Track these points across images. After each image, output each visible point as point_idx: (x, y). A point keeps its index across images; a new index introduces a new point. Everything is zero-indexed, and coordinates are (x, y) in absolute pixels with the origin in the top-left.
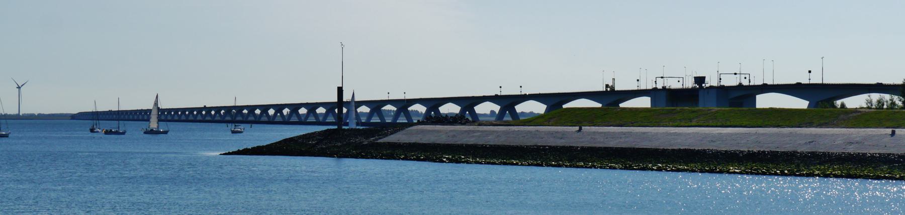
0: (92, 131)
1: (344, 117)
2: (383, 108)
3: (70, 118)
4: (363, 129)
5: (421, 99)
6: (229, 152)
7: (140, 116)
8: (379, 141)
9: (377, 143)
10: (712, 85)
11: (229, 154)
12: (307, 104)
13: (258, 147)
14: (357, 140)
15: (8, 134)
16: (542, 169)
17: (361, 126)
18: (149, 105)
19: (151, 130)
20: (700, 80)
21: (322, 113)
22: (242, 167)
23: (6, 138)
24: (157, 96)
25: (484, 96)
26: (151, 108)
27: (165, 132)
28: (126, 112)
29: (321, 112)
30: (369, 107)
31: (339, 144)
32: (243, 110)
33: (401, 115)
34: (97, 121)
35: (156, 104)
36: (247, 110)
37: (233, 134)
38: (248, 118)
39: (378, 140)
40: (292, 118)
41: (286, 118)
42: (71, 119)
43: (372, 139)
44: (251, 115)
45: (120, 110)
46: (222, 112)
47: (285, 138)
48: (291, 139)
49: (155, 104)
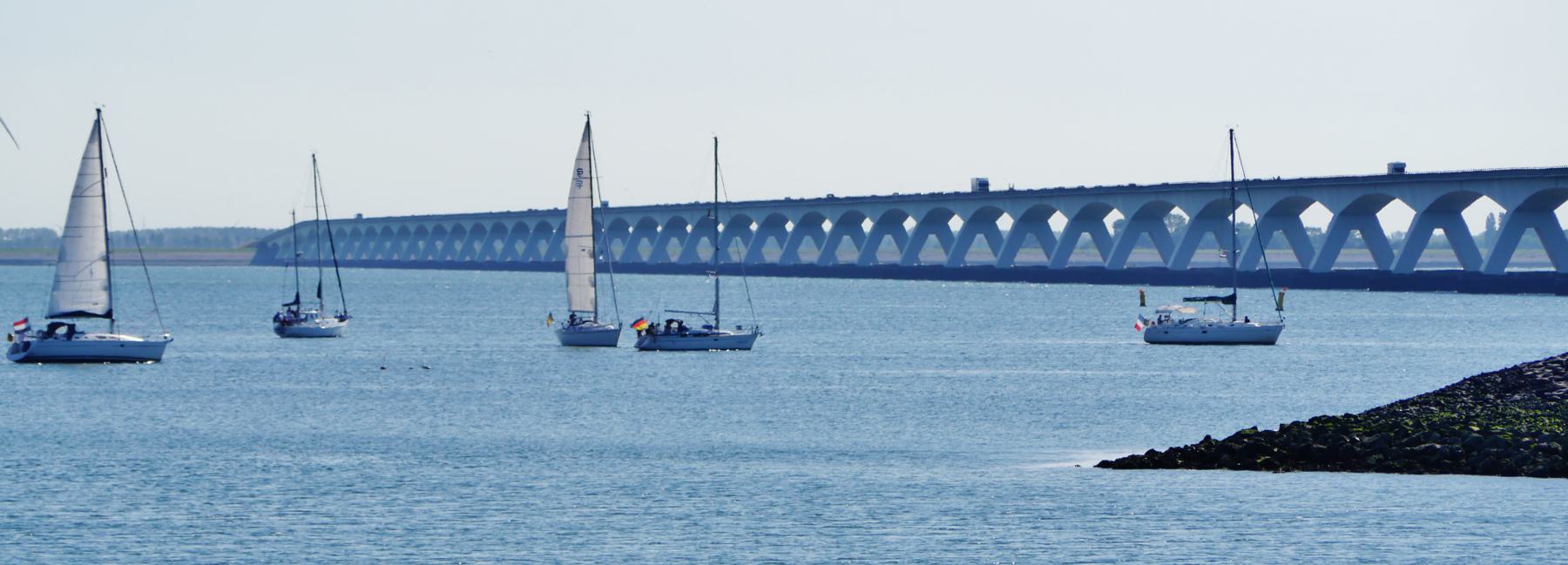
0: (288, 325)
3: (251, 254)
6: (1151, 453)
7: (645, 241)
10: (729, 200)
11: (1153, 461)
13: (1320, 423)
15: (161, 346)
16: (1513, 482)
18: (551, 194)
19: (1181, 322)
20: (360, 215)
22: (1272, 521)
24: (98, 123)
28: (157, 237)
30: (1331, 210)
34: (329, 272)
35: (583, 174)
37: (573, 351)
41: (1485, 253)
42: (256, 262)
45: (721, 199)
46: (1113, 218)
47: (1476, 372)
48: (1514, 380)
49: (579, 171)
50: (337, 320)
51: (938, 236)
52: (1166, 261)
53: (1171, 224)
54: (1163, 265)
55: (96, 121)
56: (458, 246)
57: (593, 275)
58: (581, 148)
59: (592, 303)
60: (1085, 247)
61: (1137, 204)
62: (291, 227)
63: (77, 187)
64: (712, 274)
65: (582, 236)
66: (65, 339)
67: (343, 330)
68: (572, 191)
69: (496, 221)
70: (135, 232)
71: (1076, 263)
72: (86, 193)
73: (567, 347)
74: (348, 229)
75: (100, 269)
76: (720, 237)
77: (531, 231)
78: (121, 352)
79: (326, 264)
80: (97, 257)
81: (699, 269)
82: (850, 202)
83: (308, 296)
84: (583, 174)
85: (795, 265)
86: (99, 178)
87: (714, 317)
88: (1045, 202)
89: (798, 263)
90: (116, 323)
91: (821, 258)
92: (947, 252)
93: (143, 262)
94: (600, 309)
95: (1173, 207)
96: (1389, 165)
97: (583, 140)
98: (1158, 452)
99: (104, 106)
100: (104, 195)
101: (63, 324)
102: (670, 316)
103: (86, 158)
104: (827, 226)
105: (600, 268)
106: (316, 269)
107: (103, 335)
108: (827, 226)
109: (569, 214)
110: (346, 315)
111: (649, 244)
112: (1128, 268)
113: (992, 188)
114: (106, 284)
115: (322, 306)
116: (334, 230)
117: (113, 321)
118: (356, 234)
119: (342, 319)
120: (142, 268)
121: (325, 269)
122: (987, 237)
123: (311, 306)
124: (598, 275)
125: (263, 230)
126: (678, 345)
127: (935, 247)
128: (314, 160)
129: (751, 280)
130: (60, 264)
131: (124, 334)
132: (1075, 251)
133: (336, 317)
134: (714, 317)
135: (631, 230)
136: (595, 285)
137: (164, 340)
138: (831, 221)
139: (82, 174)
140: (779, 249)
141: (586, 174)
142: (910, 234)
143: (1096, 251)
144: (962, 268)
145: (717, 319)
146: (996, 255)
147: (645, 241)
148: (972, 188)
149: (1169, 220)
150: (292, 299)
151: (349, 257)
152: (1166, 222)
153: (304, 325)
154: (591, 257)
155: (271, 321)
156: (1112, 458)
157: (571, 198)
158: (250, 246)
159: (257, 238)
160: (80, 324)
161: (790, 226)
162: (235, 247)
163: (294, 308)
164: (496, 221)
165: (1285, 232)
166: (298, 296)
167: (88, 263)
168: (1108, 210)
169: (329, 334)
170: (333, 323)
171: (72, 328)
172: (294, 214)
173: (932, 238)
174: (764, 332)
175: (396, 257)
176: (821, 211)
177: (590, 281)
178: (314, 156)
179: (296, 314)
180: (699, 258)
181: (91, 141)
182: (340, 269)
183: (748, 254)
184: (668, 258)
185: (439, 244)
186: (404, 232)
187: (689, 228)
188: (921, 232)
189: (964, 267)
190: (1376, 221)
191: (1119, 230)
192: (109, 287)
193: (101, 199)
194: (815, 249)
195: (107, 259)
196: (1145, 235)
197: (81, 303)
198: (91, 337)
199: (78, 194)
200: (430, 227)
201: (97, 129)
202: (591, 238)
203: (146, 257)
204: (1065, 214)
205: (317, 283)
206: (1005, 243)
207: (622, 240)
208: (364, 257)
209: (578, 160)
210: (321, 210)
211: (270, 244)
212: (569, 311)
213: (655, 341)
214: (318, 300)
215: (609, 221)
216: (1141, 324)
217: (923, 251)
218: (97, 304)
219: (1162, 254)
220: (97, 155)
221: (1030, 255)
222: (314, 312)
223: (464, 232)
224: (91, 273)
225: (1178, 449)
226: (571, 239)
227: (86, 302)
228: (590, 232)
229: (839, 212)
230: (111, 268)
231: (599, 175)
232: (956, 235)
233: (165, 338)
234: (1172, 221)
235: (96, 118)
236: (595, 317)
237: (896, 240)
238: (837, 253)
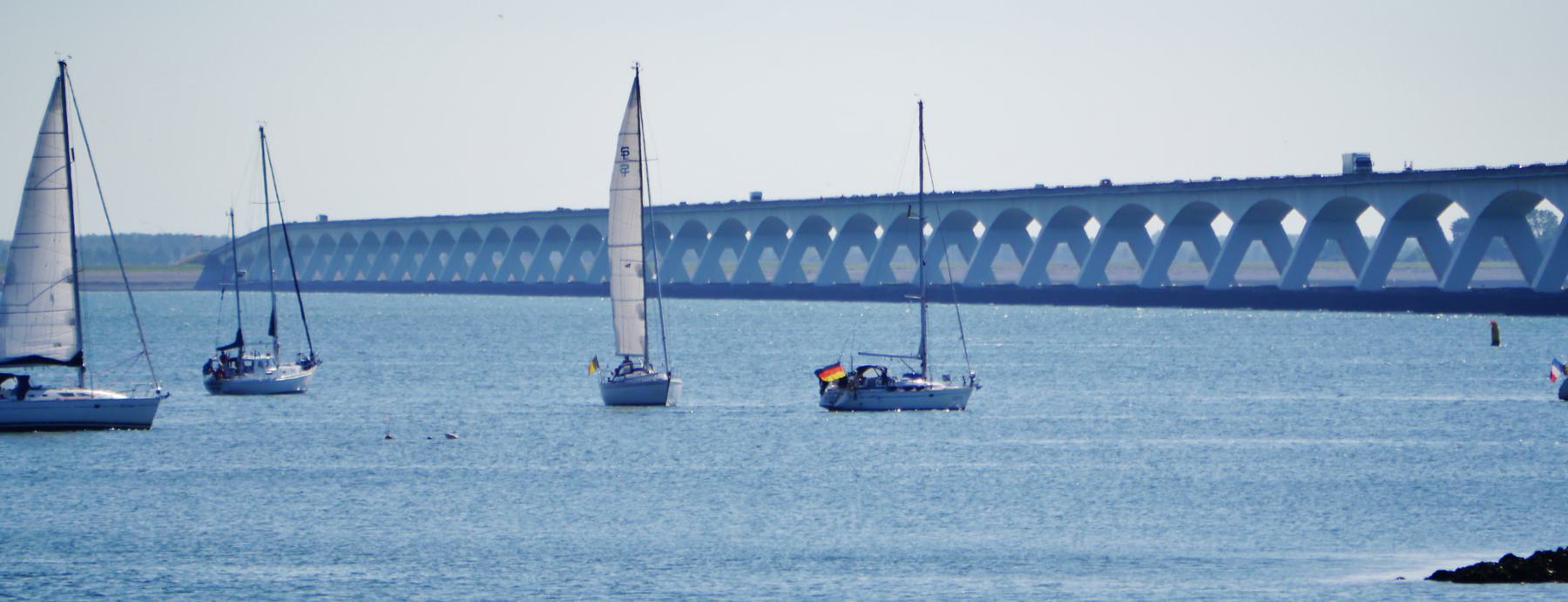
3: (197, 273)
5: (589, 210)
6: (1509, 559)
12: (1480, 175)
15: (151, 405)
23: (139, 434)
24: (61, 82)
25: (1272, 178)
26: (599, 199)
34: (287, 299)
35: (629, 157)
45: (927, 190)
46: (1451, 217)
49: (624, 151)
50: (299, 367)
51: (1196, 244)
52: (1529, 278)
53: (1537, 225)
54: (1526, 285)
55: (58, 78)
56: (498, 260)
57: (643, 302)
58: (626, 122)
59: (641, 342)
60: (1412, 258)
61: (1487, 196)
62: (262, 230)
63: (32, 175)
64: (915, 301)
65: (628, 246)
66: (15, 397)
67: (307, 382)
68: (615, 180)
69: (687, 218)
70: (113, 237)
71: (1396, 282)
72: (40, 186)
73: (612, 407)
74: (315, 237)
75: (65, 293)
76: (926, 249)
77: (572, 240)
78: (96, 415)
79: (282, 286)
80: (60, 277)
81: (896, 293)
82: (1011, 196)
83: (256, 332)
84: (629, 157)
85: (988, 287)
86: (63, 162)
87: (921, 361)
88: (1435, 190)
89: (993, 283)
90: (87, 374)
91: (1084, 276)
92: (1208, 266)
93: (128, 286)
94: (931, 352)
95: (1538, 199)
96: (1344, 157)
97: (630, 105)
98: (1518, 558)
99: (70, 57)
100: (70, 187)
101: (11, 376)
102: (862, 362)
103: (44, 133)
104: (1034, 229)
105: (650, 291)
106: (268, 294)
107: (69, 391)
108: (1034, 229)
109: (610, 213)
110: (313, 359)
111: (775, 256)
112: (1473, 289)
113: (1376, 168)
114: (73, 315)
115: (276, 347)
116: (294, 238)
117: (83, 369)
118: (326, 243)
119: (306, 365)
120: (294, 295)
121: (280, 295)
122: (1265, 243)
123: (258, 348)
124: (649, 301)
125: (213, 238)
126: (874, 403)
127: (1192, 260)
128: (263, 137)
129: (966, 309)
130: (7, 288)
131: (99, 388)
132: (1396, 265)
133: (297, 364)
134: (921, 361)
135: (790, 234)
136: (645, 316)
137: (156, 395)
138: (1040, 221)
139: (39, 157)
140: (964, 262)
141: (633, 155)
142: (1155, 241)
143: (1427, 265)
144: (1163, 289)
145: (923, 365)
146: (1280, 270)
147: (811, 252)
148: (1344, 169)
149: (1534, 219)
150: (232, 339)
151: (318, 276)
152: (1530, 221)
153: (249, 377)
154: (639, 275)
155: (199, 372)
156: (1452, 566)
157: (614, 190)
158: (195, 261)
159: (207, 251)
160: (38, 375)
161: (979, 230)
162: (172, 263)
163: (234, 353)
164: (687, 218)
165: (1507, 239)
166: (239, 334)
167: (47, 286)
168: (1443, 204)
169: (289, 389)
170: (296, 372)
171: (24, 380)
172: (232, 215)
173: (1188, 247)
174: (980, 384)
175: (407, 277)
176: (1026, 207)
177: (640, 313)
178: (261, 130)
179: (239, 360)
180: (847, 275)
181: (51, 107)
182: (133, 293)
183: (825, 269)
184: (804, 277)
185: (470, 258)
186: (418, 240)
187: (833, 233)
188: (1391, 237)
189: (1233, 287)
190: (1437, 223)
191: (1460, 234)
192: (77, 321)
193: (65, 193)
194: (1017, 262)
195: (74, 279)
196: (1499, 241)
197: (35, 344)
198: (52, 394)
199: (34, 186)
200: (483, 232)
201: (60, 93)
202: (641, 248)
203: (133, 275)
204: (1382, 211)
205: (268, 315)
206: (1293, 255)
207: (736, 251)
208: (360, 277)
209: (623, 134)
210: (274, 208)
211: (223, 259)
212: (617, 354)
213: (855, 397)
214: (271, 339)
215: (655, 222)
216: (1556, 372)
217: (1172, 266)
218: (59, 345)
219: (1523, 267)
220: (60, 128)
221: (1331, 271)
222: (263, 357)
223: (565, 237)
224: (52, 298)
225: (1549, 553)
226: (614, 249)
227: (45, 343)
228: (639, 240)
229: (1112, 207)
230: (81, 293)
231: (648, 158)
232: (1222, 242)
233: (158, 392)
234: (1539, 220)
235: (58, 73)
236: (646, 362)
237: (1135, 252)
238: (1049, 267)
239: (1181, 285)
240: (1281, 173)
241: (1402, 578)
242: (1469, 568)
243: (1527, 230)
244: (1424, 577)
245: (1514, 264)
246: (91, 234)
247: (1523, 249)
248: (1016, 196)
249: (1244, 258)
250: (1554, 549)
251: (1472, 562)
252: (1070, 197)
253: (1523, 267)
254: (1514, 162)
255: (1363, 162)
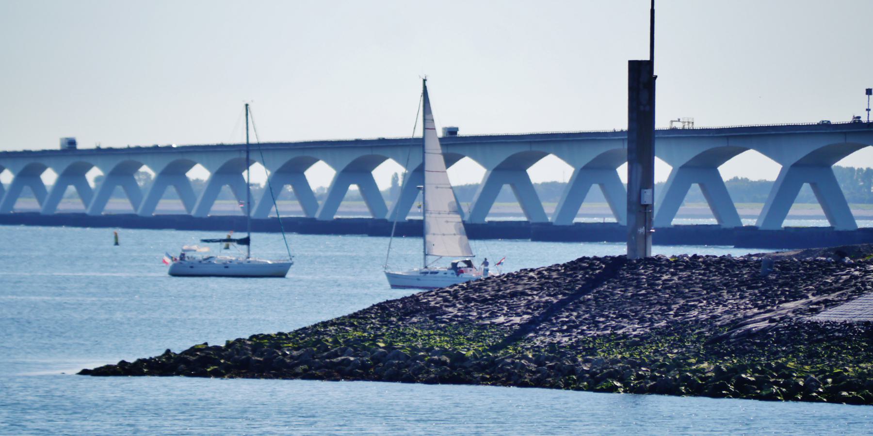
1: (657, 205)
2: (845, 163)
4: (745, 262)
6: (123, 363)
8: (821, 317)
9: (814, 325)
12: (111, 152)
13: (258, 340)
14: (720, 309)
17: (738, 245)
21: (554, 184)
27: (278, 272)
29: (549, 179)
31: (634, 329)
32: (190, 165)
33: (501, 195)
36: (207, 166)
38: (155, 203)
39: (816, 311)
40: (585, 207)
41: (390, 204)
43: (792, 305)
44: (226, 188)
45: (253, 140)
46: (93, 175)
52: (136, 208)
53: (140, 180)
54: (185, 213)
60: (71, 197)
88: (188, 157)
95: (140, 165)
152: (136, 177)
156: (91, 367)
165: (124, 187)
168: (89, 167)
216: (168, 260)
225: (144, 360)
239: (599, 243)
240: (133, 145)
241: (63, 373)
242: (101, 368)
243: (134, 182)
244: (75, 373)
245: (180, 202)
246: (660, 182)
247: (133, 192)
248: (191, 150)
249: (492, 207)
250: (147, 358)
251: (102, 365)
252: (530, 142)
253: (186, 204)
254: (826, 118)
255: (72, 143)
